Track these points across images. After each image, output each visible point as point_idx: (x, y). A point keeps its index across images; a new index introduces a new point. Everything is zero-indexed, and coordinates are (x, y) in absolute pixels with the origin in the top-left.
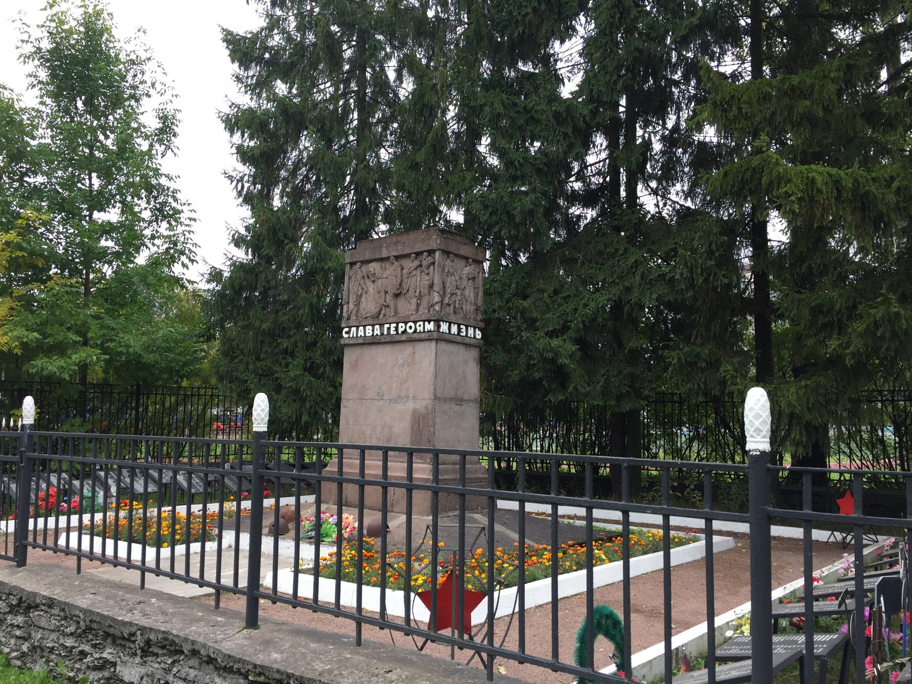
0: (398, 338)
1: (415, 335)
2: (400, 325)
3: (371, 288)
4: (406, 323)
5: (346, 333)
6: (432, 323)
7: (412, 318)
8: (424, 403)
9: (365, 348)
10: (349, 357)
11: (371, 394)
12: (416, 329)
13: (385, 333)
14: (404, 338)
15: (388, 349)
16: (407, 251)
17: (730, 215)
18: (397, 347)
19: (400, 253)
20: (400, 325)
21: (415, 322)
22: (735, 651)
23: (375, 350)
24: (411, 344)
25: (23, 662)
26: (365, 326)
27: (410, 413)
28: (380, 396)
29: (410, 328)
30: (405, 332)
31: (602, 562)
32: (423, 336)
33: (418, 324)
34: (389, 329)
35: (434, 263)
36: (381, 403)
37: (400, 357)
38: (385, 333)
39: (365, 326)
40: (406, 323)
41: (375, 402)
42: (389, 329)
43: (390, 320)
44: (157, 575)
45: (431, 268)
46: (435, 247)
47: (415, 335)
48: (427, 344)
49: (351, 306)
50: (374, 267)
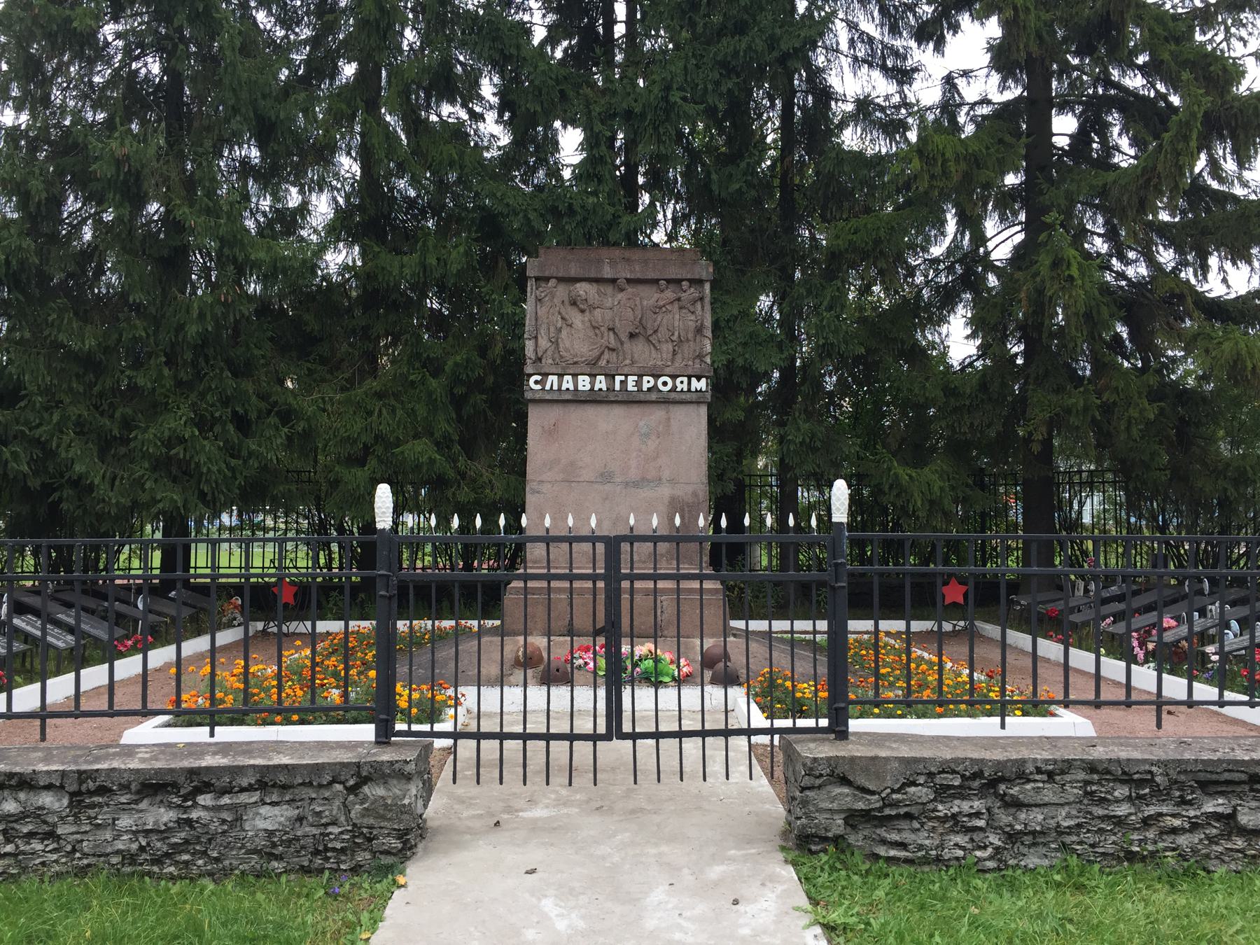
0: (642, 397)
1: (673, 395)
2: (645, 379)
3: (577, 319)
4: (656, 377)
5: (536, 382)
6: (704, 380)
7: (668, 370)
8: (690, 489)
9: (572, 407)
10: (537, 420)
11: (587, 475)
12: (675, 387)
13: (617, 387)
14: (653, 396)
15: (618, 411)
16: (651, 275)
17: (911, 271)
18: (636, 410)
19: (639, 276)
20: (645, 379)
21: (674, 377)
22: (1145, 697)
23: (591, 412)
24: (663, 406)
25: (1000, 860)
26: (575, 376)
27: (666, 502)
28: (606, 477)
29: (665, 384)
30: (654, 389)
31: (19, 686)
32: (688, 397)
33: (679, 380)
34: (623, 383)
35: (701, 299)
36: (608, 487)
37: (641, 424)
38: (617, 387)
39: (575, 376)
40: (656, 377)
41: (596, 486)
42: (623, 383)
43: (626, 371)
44: (1252, 707)
45: (699, 305)
46: (704, 276)
47: (673, 395)
48: (691, 408)
49: (544, 343)
50: (582, 289)
